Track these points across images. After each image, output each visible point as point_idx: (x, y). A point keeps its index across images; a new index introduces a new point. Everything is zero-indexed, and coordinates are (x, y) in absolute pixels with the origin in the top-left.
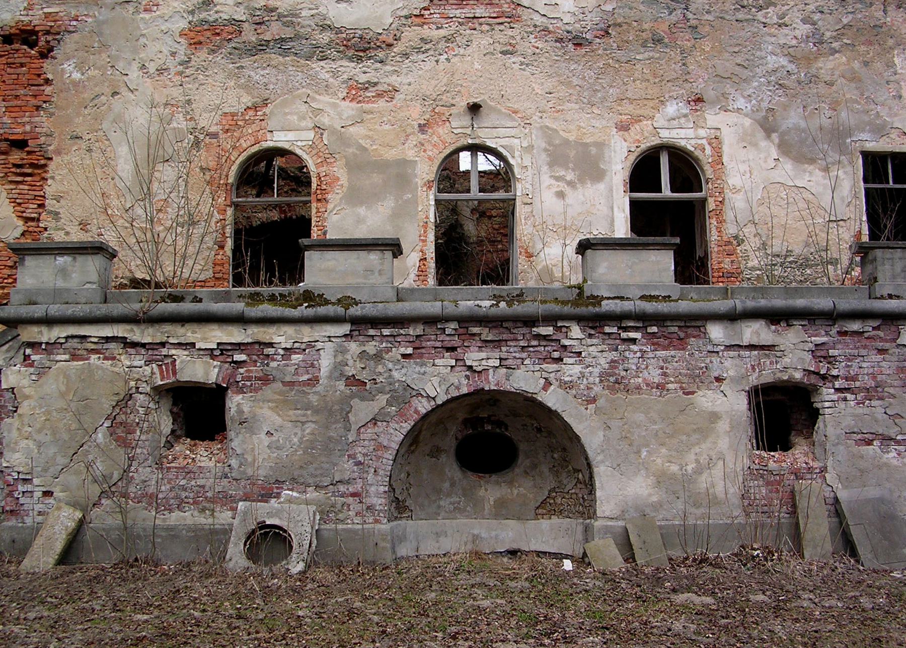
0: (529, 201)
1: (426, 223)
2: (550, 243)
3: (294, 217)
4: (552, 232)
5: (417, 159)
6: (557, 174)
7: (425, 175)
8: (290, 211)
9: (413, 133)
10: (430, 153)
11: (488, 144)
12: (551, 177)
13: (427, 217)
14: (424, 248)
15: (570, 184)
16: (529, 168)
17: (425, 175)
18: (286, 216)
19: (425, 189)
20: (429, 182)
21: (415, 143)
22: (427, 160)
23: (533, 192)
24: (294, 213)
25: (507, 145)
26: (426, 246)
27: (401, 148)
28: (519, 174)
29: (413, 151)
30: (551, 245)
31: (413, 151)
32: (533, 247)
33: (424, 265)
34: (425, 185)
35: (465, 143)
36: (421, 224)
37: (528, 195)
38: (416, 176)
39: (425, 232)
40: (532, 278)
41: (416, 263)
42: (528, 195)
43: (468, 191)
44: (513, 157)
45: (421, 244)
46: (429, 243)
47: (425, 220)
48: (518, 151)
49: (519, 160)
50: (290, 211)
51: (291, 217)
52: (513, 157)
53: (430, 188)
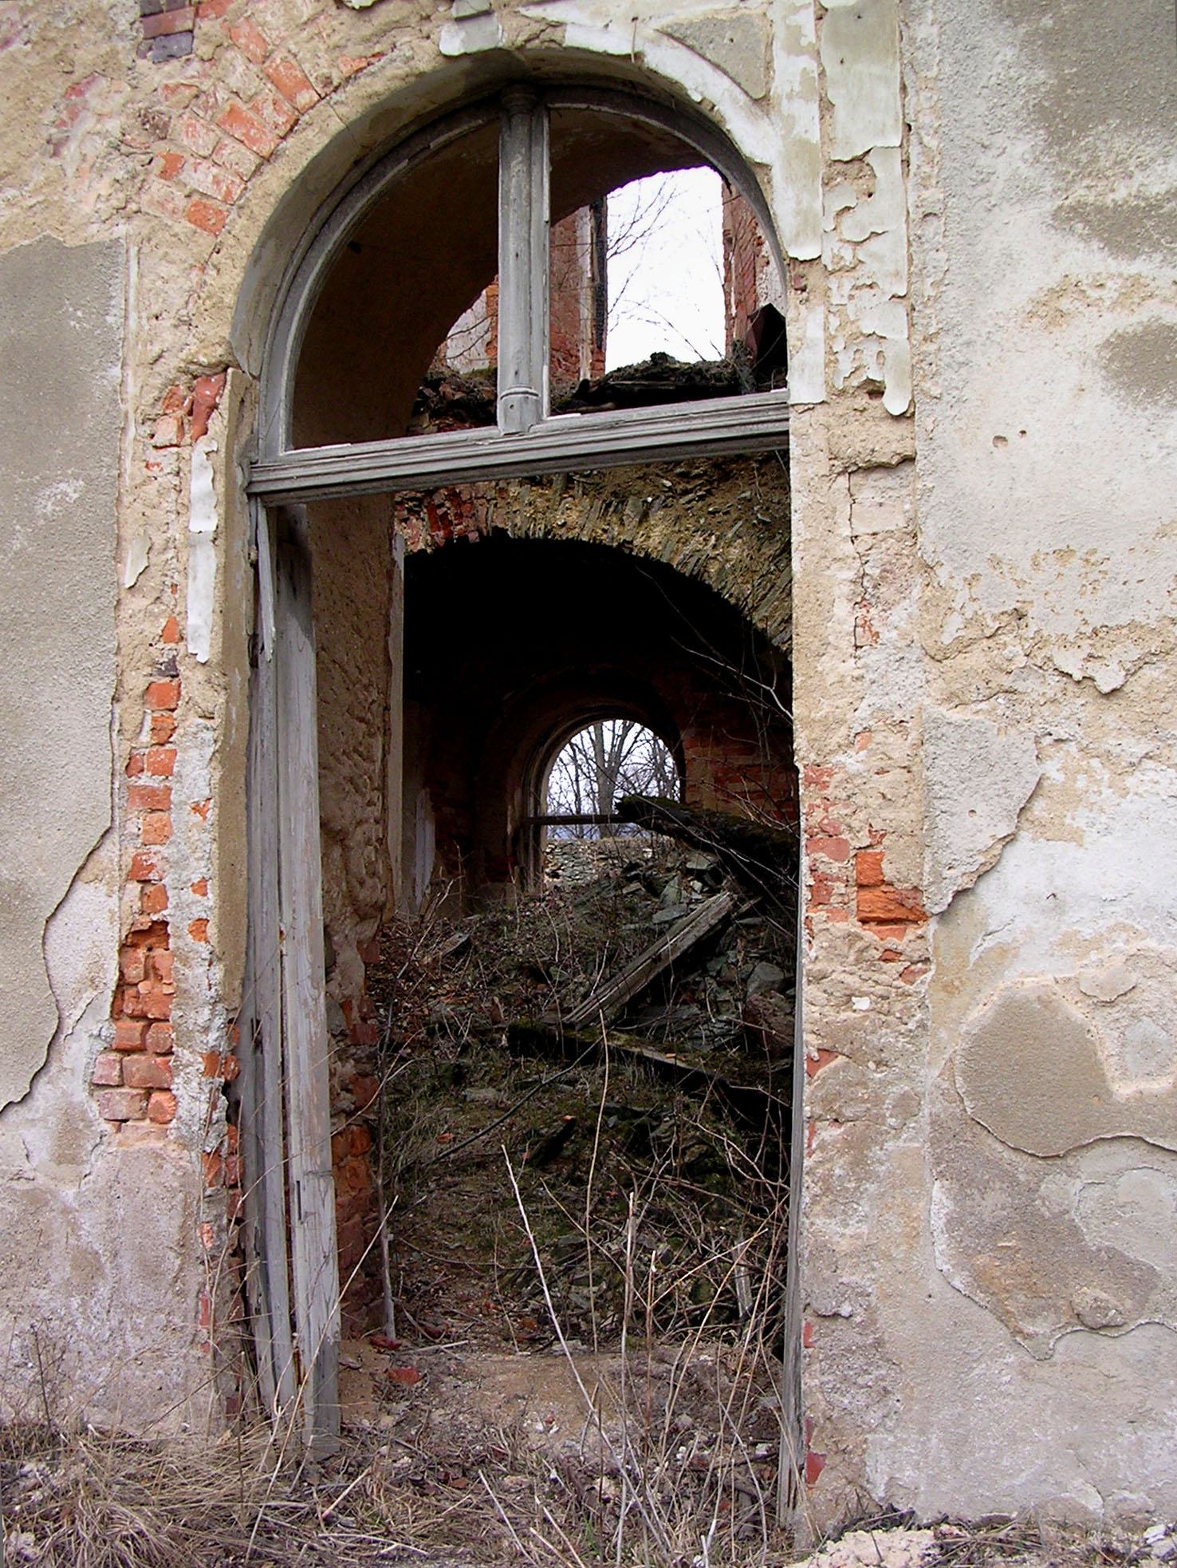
0: (888, 442)
1: (171, 670)
2: (1074, 799)
3: (473, 537)
4: (1079, 704)
5: (122, 229)
6: (1122, 192)
7: (168, 336)
8: (459, 516)
9: (106, 67)
10: (200, 178)
11: (574, 38)
12: (1068, 217)
13: (174, 633)
14: (159, 853)
15: (1165, 163)
16: (886, 171)
17: (168, 336)
18: (448, 538)
19: (167, 430)
20: (196, 374)
21: (113, 126)
22: (183, 227)
23: (918, 367)
24: (471, 522)
25: (712, 24)
26: (162, 835)
27: (39, 177)
28: (808, 225)
29: (103, 187)
30: (1079, 819)
31: (103, 187)
32: (922, 837)
33: (152, 971)
34: (169, 399)
35: (425, 64)
36: (136, 681)
37: (875, 391)
38: (111, 348)
39: (164, 736)
40: (907, 1106)
41: (98, 964)
42: (875, 391)
43: (480, 412)
44: (762, 102)
45: (136, 822)
46: (182, 818)
47: (163, 652)
48: (795, 48)
49: (807, 114)
50: (459, 516)
51: (463, 538)
52: (762, 102)
53: (197, 415)
